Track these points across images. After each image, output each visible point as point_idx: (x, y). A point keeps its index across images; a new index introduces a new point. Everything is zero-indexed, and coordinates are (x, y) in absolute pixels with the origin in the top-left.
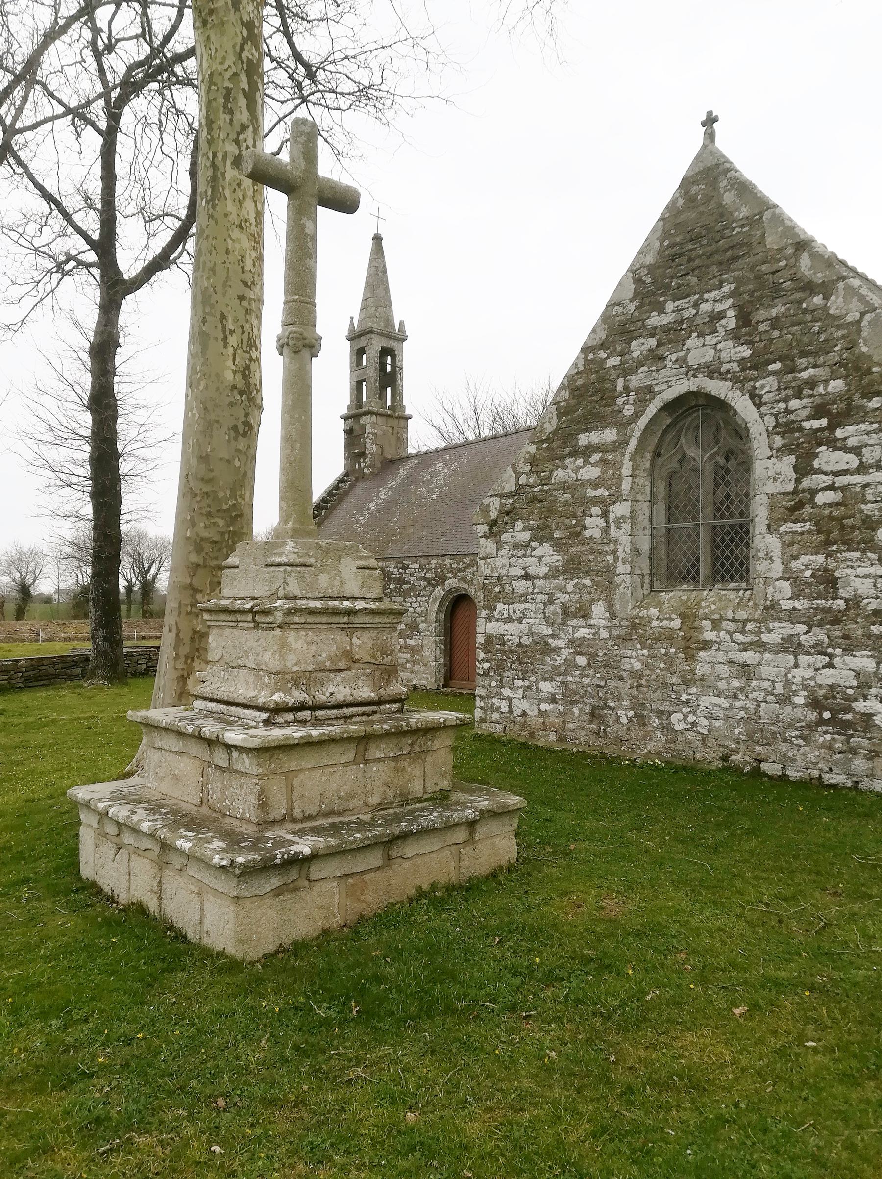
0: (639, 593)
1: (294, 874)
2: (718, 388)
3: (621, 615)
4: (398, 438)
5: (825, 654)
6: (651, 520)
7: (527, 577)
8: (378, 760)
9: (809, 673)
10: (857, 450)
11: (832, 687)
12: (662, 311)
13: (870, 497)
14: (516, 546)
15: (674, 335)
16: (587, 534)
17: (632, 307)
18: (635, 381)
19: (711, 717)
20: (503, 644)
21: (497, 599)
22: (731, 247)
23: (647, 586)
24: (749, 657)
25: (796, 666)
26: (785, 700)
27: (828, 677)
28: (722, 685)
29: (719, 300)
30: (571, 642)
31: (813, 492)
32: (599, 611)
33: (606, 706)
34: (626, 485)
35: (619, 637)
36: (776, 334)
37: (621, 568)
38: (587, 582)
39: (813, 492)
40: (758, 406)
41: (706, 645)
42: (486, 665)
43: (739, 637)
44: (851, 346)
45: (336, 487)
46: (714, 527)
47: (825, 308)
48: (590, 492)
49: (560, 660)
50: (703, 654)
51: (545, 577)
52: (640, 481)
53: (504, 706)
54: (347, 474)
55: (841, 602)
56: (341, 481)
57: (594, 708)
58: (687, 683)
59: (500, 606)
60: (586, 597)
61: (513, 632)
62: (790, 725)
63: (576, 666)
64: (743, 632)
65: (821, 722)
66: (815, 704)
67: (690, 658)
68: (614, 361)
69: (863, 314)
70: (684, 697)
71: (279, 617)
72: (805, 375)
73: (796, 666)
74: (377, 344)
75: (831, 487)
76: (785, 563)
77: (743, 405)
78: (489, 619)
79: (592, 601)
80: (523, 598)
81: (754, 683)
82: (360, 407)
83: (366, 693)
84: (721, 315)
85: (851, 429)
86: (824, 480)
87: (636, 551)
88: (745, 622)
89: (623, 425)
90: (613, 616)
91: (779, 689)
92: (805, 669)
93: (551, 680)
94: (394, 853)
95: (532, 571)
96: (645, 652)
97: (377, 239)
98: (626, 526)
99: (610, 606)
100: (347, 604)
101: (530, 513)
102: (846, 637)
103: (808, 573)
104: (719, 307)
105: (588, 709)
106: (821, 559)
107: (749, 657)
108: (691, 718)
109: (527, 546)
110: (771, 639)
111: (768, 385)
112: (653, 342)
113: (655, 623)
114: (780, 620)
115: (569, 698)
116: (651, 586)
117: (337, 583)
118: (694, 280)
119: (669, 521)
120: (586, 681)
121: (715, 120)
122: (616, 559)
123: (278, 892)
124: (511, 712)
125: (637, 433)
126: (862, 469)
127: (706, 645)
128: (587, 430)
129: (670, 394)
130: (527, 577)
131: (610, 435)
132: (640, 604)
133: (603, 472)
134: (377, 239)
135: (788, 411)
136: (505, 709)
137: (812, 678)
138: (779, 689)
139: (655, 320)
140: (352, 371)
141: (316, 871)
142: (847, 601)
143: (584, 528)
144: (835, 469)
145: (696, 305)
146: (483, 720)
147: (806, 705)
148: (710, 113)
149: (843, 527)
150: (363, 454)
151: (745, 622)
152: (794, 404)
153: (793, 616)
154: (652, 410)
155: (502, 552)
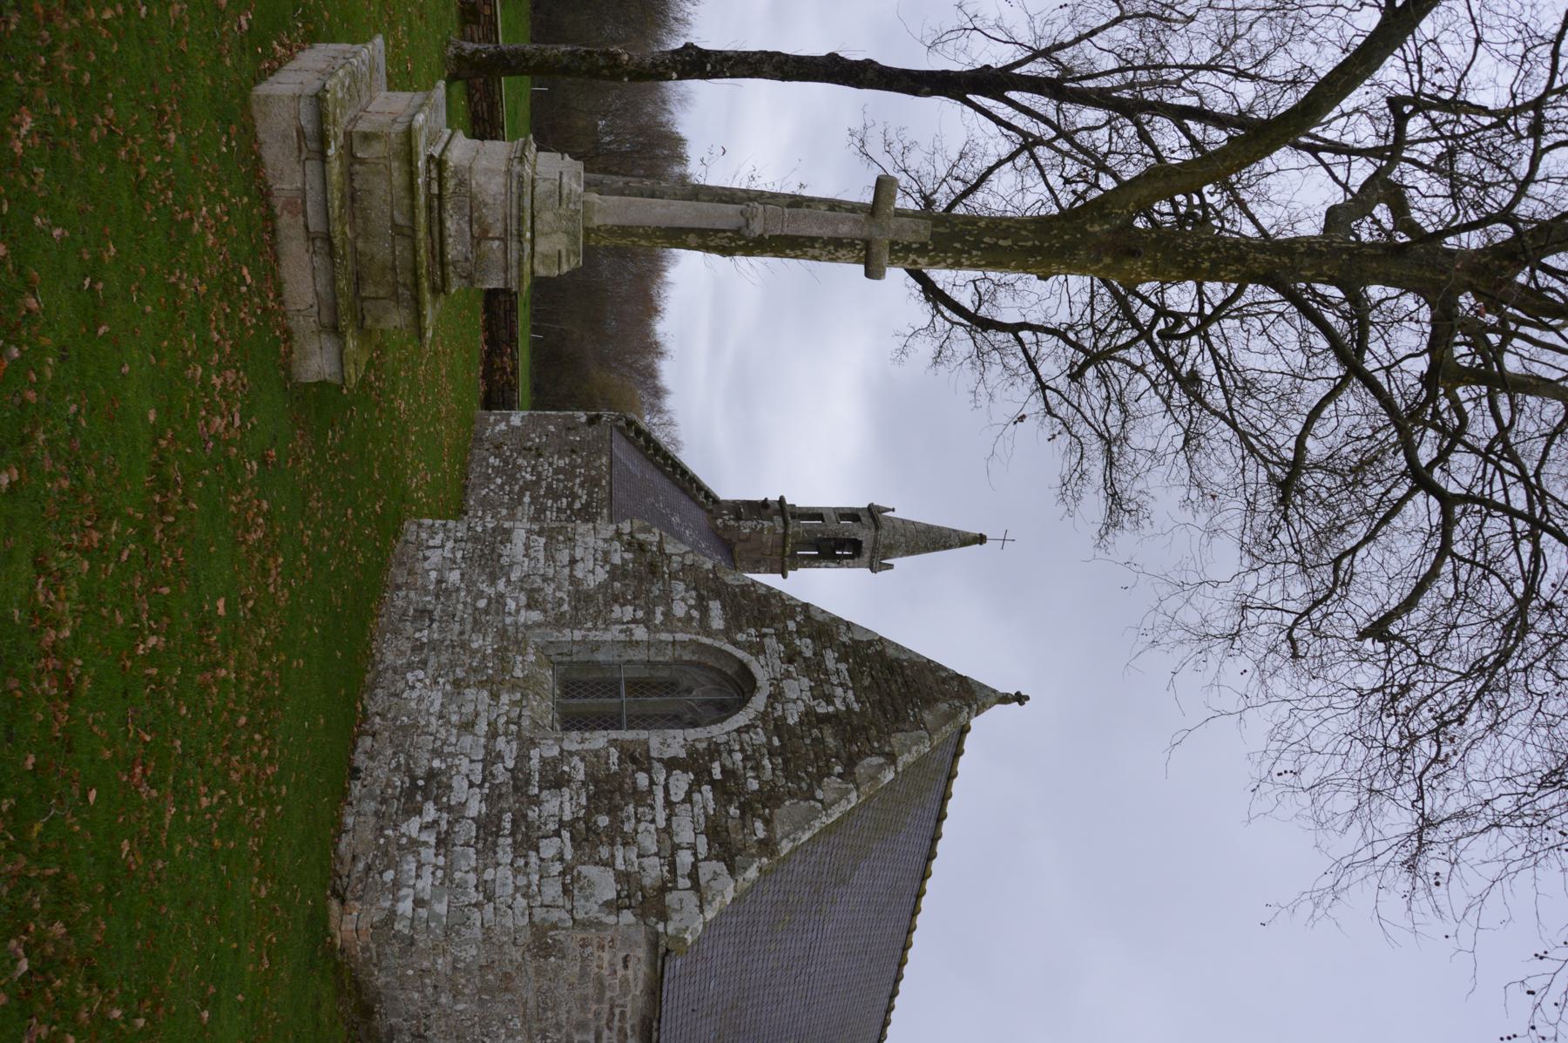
0: (552, 651)
1: (314, 146)
2: (759, 702)
3: (528, 634)
4: (758, 562)
5: (484, 780)
6: (629, 662)
7: (573, 562)
8: (393, 247)
9: (464, 770)
10: (688, 798)
11: (450, 787)
12: (838, 660)
13: (640, 810)
14: (606, 553)
15: (814, 667)
16: (616, 608)
17: (845, 639)
18: (771, 642)
19: (420, 699)
20: (502, 542)
21: (551, 538)
22: (896, 710)
23: (559, 658)
24: (482, 727)
25: (472, 761)
26: (436, 753)
27: (460, 784)
28: (454, 707)
29: (843, 699)
30: (501, 596)
31: (648, 771)
32: (536, 616)
33: (432, 621)
34: (665, 636)
35: (506, 631)
36: (808, 741)
37: (578, 635)
38: (566, 607)
39: (648, 771)
40: (738, 731)
41: (495, 696)
42: (479, 529)
43: (503, 719)
44: (791, 795)
45: (700, 487)
46: (620, 715)
47: (829, 775)
48: (659, 610)
49: (484, 587)
50: (485, 694)
51: (571, 576)
52: (669, 652)
53: (437, 541)
54: (716, 501)
55: (536, 791)
56: (708, 494)
57: (431, 612)
58: (457, 683)
59: (542, 540)
60: (549, 606)
61: (516, 547)
62: (409, 756)
63: (475, 599)
64: (507, 723)
65: (414, 779)
66: (432, 774)
67: (481, 685)
68: (792, 626)
69: (821, 801)
70: (441, 680)
71: (517, 168)
72: (766, 762)
73: (472, 761)
74: (864, 535)
75: (652, 782)
76: (577, 753)
77: (741, 719)
78: (529, 531)
79: (545, 611)
80: (550, 558)
81: (454, 731)
82: (793, 517)
83: (452, 253)
84: (829, 700)
85: (710, 795)
86: (661, 777)
87: (597, 646)
88: (518, 724)
89: (727, 633)
90: (527, 627)
91: (446, 749)
92: (467, 768)
93: (462, 580)
94: (318, 243)
95: (580, 565)
96: (489, 651)
97: (981, 539)
98: (622, 637)
99: (539, 625)
100: (528, 235)
101: (641, 564)
102: (500, 796)
103: (566, 768)
104: (838, 702)
105: (430, 607)
106: (581, 776)
107: (482, 727)
108: (419, 685)
109: (606, 561)
110: (501, 743)
111: (759, 737)
112: (808, 653)
113: (520, 658)
114: (519, 749)
115: (443, 591)
116: (560, 663)
117: (547, 229)
118: (867, 682)
119: (628, 682)
120: (460, 607)
121: (1021, 703)
122: (589, 630)
123: (301, 132)
124: (429, 547)
125: (717, 644)
126: (669, 803)
127: (495, 696)
128: (724, 607)
129: (755, 667)
130: (573, 562)
131: (717, 623)
132: (540, 650)
133: (680, 620)
134: (981, 539)
135: (730, 752)
136: (431, 543)
137: (458, 773)
138: (446, 749)
139: (830, 657)
140: (835, 509)
141: (312, 167)
142: (537, 796)
143: (622, 605)
144: (671, 786)
145: (841, 685)
146: (420, 526)
147: (431, 768)
148: (1027, 698)
149: (612, 792)
150: (738, 518)
151: (518, 724)
152: (738, 756)
153: (523, 757)
154: (740, 654)
155: (600, 543)
